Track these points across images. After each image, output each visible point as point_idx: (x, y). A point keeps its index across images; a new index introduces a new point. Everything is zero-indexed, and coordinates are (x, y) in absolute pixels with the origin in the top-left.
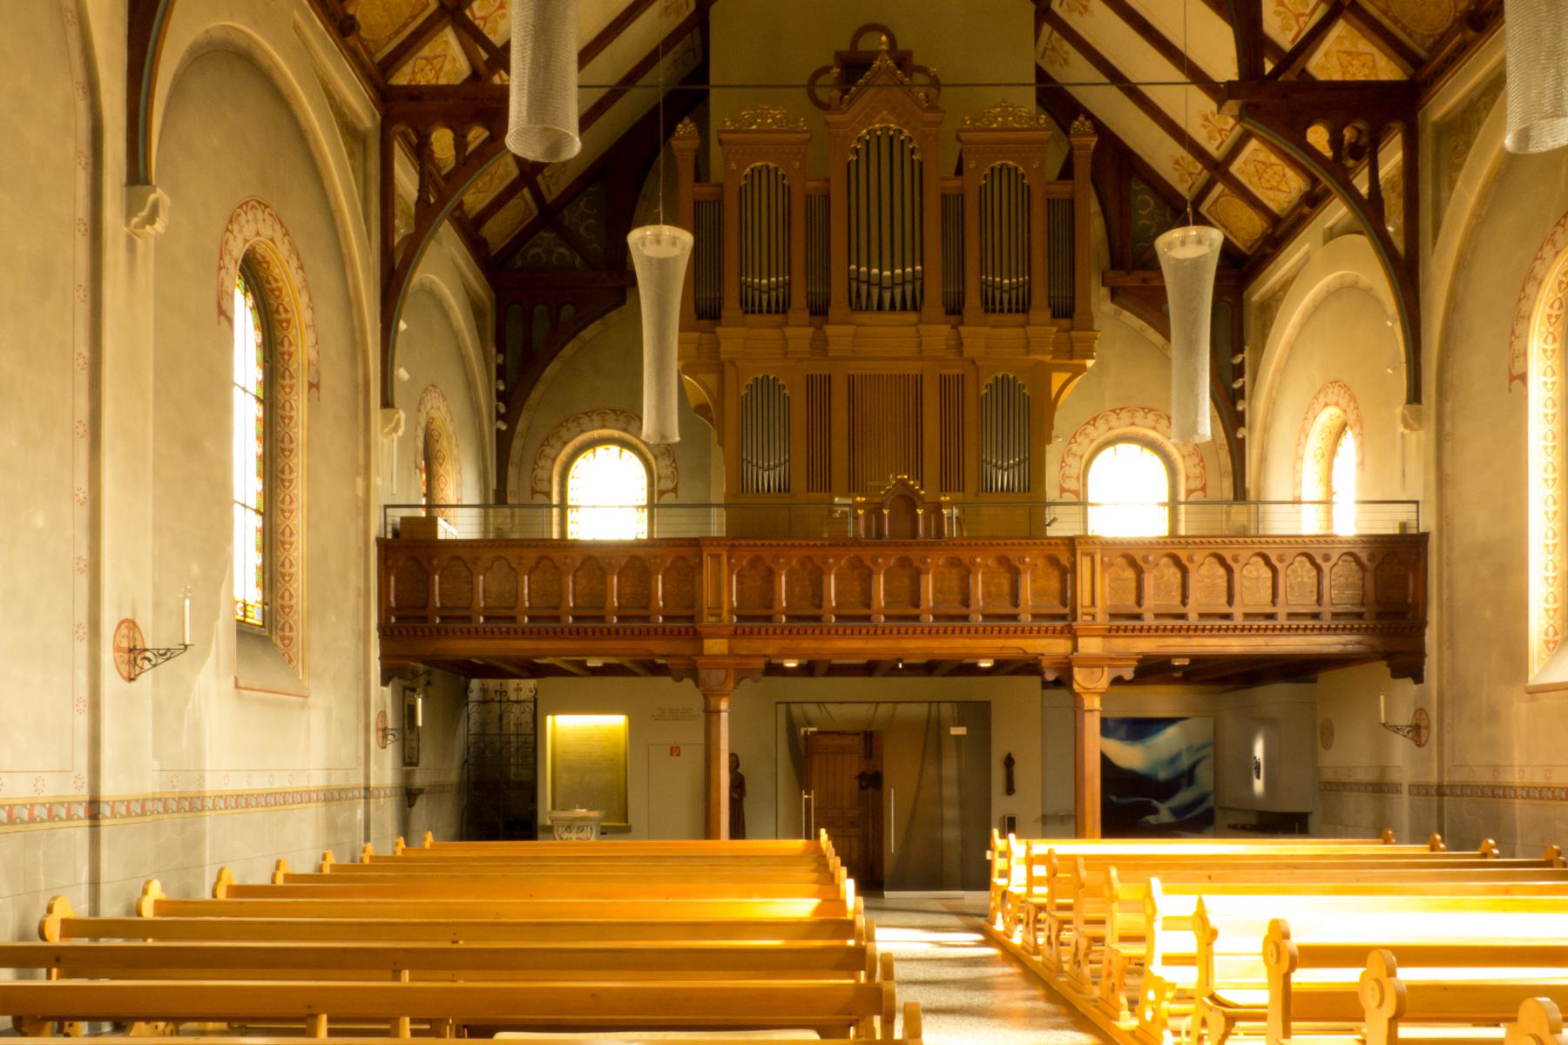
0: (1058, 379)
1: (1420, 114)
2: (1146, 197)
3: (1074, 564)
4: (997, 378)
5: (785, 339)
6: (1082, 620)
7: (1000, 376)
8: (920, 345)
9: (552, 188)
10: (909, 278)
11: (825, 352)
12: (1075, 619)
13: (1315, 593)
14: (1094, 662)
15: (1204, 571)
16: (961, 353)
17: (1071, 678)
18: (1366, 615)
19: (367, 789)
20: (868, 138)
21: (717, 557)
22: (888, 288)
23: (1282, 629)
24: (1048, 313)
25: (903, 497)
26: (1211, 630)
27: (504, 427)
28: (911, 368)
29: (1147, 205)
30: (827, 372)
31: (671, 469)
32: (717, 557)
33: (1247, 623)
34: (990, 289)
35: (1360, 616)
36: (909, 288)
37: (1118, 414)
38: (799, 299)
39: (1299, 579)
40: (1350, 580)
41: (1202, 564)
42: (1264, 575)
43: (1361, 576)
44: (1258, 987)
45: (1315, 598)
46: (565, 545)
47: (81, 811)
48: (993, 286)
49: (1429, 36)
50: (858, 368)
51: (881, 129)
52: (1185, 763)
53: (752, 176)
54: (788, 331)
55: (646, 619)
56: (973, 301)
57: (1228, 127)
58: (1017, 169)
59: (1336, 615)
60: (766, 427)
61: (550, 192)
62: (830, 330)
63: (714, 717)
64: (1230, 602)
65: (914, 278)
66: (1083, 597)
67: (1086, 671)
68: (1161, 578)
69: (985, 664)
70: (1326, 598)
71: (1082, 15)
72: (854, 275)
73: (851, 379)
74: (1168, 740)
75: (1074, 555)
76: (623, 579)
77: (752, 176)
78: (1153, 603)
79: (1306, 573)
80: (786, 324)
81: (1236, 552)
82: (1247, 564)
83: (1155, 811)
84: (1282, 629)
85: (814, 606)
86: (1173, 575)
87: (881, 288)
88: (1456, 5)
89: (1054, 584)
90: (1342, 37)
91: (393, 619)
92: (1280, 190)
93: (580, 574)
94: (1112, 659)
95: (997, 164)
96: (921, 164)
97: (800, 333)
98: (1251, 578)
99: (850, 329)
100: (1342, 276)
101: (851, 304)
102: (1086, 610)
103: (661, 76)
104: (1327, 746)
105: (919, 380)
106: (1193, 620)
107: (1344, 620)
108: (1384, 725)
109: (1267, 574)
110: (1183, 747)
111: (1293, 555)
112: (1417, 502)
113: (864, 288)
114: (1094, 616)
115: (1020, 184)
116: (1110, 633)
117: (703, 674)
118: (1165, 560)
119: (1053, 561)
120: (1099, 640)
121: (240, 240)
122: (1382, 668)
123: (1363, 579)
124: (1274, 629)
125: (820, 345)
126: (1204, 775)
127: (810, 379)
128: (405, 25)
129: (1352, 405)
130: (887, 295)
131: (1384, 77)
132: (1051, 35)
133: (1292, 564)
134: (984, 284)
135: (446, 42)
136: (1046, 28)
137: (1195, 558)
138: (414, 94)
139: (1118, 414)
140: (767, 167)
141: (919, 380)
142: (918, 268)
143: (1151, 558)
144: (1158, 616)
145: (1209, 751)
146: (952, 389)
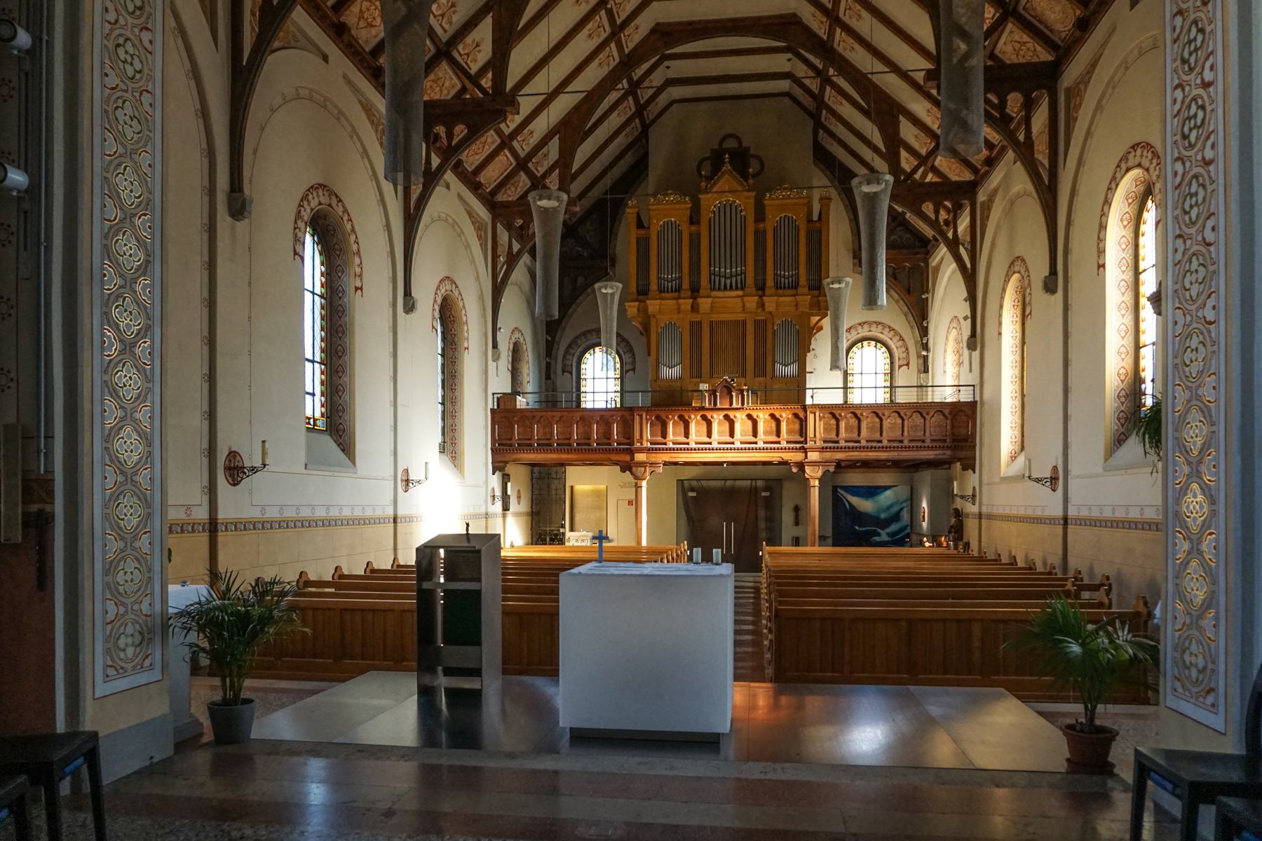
3: (806, 417)
16: (764, 310)
17: (804, 472)
19: (487, 514)
21: (641, 416)
25: (726, 387)
27: (550, 339)
28: (740, 317)
30: (699, 319)
31: (631, 360)
32: (641, 416)
33: (911, 445)
46: (327, 757)
47: (392, 520)
50: (715, 317)
52: (895, 509)
54: (681, 301)
56: (770, 283)
62: (700, 300)
65: (742, 273)
66: (810, 433)
70: (928, 433)
72: (712, 272)
73: (711, 322)
74: (887, 497)
75: (806, 412)
80: (679, 298)
83: (879, 535)
86: (854, 421)
89: (797, 426)
95: (783, 215)
96: (745, 217)
99: (710, 300)
103: (628, 160)
105: (744, 322)
106: (863, 443)
107: (939, 442)
112: (974, 386)
113: (717, 278)
116: (822, 450)
117: (634, 469)
121: (309, 210)
124: (902, 447)
125: (695, 308)
126: (905, 515)
127: (692, 323)
128: (502, 174)
130: (728, 281)
131: (968, 179)
134: (775, 274)
138: (506, 205)
141: (744, 322)
142: (743, 268)
146: (761, 326)
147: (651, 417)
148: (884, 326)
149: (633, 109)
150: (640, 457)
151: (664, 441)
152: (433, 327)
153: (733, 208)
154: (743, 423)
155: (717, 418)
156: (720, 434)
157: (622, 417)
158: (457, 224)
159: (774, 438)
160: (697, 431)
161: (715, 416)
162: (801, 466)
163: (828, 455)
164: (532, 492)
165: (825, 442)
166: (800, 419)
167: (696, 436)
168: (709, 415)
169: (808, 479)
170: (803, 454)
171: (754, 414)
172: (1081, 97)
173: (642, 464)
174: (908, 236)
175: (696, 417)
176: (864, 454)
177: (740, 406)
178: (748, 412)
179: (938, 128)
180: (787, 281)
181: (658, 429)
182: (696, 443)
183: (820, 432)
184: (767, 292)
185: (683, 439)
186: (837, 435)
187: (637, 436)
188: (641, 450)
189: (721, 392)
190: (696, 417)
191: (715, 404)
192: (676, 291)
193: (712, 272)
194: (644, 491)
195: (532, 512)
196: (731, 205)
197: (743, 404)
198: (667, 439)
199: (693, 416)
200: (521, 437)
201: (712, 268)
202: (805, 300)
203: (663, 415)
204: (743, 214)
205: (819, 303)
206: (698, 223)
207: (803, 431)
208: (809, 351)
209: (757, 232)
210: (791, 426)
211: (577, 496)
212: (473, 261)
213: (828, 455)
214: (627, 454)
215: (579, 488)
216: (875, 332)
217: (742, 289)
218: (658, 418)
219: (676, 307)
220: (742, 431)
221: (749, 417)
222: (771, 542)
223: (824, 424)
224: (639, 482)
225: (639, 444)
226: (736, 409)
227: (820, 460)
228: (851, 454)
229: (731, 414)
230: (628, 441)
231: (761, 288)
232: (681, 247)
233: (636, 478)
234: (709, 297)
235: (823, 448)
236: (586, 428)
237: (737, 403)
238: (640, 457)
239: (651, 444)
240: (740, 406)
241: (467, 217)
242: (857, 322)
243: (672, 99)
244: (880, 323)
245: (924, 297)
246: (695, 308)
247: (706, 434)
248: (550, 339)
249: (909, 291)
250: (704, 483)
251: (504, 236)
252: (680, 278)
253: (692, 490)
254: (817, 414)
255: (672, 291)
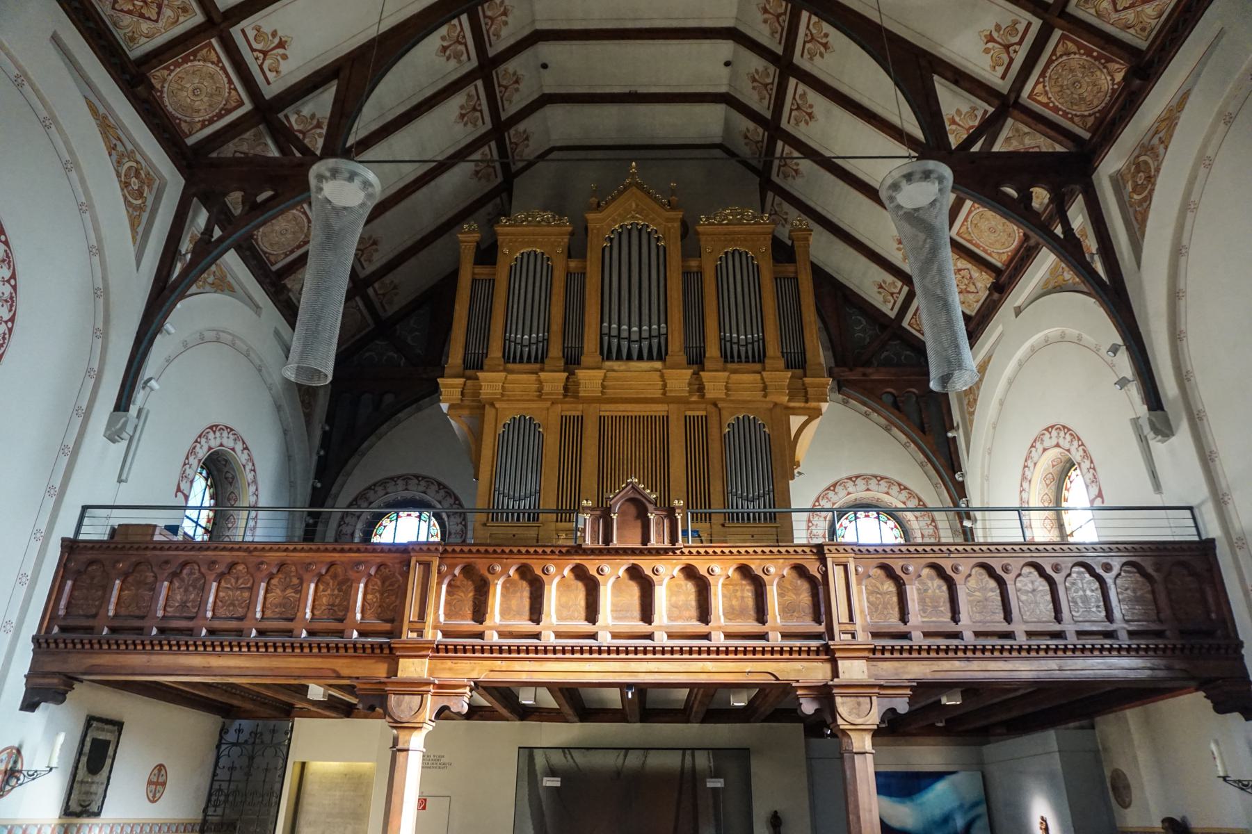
0: (796, 422)
1: (1094, 177)
2: (859, 318)
3: (825, 575)
4: (738, 418)
5: (540, 382)
6: (841, 639)
7: (741, 417)
8: (665, 386)
9: (387, 307)
10: (654, 333)
11: (576, 396)
12: (832, 638)
13: (1102, 608)
14: (858, 689)
15: (972, 582)
16: (703, 396)
17: (833, 711)
18: (1168, 633)
20: (620, 230)
22: (637, 341)
23: (1074, 650)
24: (781, 363)
26: (992, 651)
28: (659, 410)
29: (860, 322)
30: (579, 413)
31: (460, 527)
32: (427, 566)
34: (728, 344)
35: (1159, 634)
36: (655, 341)
37: (854, 482)
38: (555, 351)
39: (1081, 593)
40: (1139, 593)
41: (970, 575)
42: (1041, 588)
43: (1150, 588)
44: (446, 386)
45: (1103, 614)
48: (731, 341)
49: (1090, 115)
50: (609, 410)
51: (631, 224)
53: (522, 259)
55: (340, 633)
56: (713, 350)
57: (897, 291)
58: (747, 253)
59: (1132, 634)
60: (524, 472)
61: (385, 311)
62: (581, 374)
63: (401, 756)
64: (1008, 617)
67: (850, 701)
68: (926, 590)
69: (739, 702)
71: (807, 124)
73: (601, 419)
74: (939, 797)
76: (321, 587)
77: (522, 259)
78: (920, 619)
79: (1090, 588)
81: (1006, 561)
82: (1019, 575)
84: (1074, 650)
85: (531, 620)
86: (937, 588)
87: (630, 341)
88: (1113, 80)
89: (805, 598)
90: (1010, 137)
91: (56, 630)
92: (969, 292)
93: (274, 581)
94: (881, 687)
95: (730, 249)
96: (665, 248)
97: (554, 380)
98: (1028, 592)
100: (1046, 336)
101: (602, 353)
102: (843, 628)
104: (1125, 805)
108: (1225, 778)
109: (1043, 586)
110: (956, 804)
111: (1070, 565)
114: (854, 637)
115: (750, 265)
116: (874, 654)
118: (926, 572)
119: (800, 570)
120: (863, 663)
122: (1194, 704)
123: (1153, 592)
125: (570, 390)
127: (564, 420)
128: (292, 252)
129: (1076, 443)
132: (774, 199)
133: (1069, 575)
134: (722, 340)
135: (266, 145)
136: (770, 195)
137: (960, 568)
139: (854, 482)
140: (535, 252)
143: (911, 569)
144: (927, 635)
145: (982, 809)
146: (696, 429)
147: (452, 567)
148: (891, 482)
149: (474, 63)
150: (411, 668)
151: (478, 628)
152: (179, 490)
153: (645, 237)
154: (672, 592)
155: (611, 574)
156: (618, 611)
157: (380, 566)
158: (29, 80)
159: (752, 626)
160: (561, 607)
161: (607, 570)
162: (825, 694)
163: (888, 670)
164: (214, 774)
165: (875, 635)
166: (811, 580)
167: (560, 618)
168: (591, 566)
169: (844, 732)
170: (828, 666)
171: (701, 567)
172: (974, 395)
173: (416, 687)
174: (908, 353)
175: (560, 569)
176: (975, 665)
177: (667, 545)
178: (685, 561)
179: (905, 259)
180: (743, 349)
181: (467, 596)
182: (559, 635)
183: (862, 612)
184: (707, 364)
185: (528, 626)
186: (904, 617)
187: (411, 612)
188: (416, 650)
189: (622, 513)
190: (560, 569)
191: (608, 539)
192: (536, 361)
193: (606, 331)
194: (413, 766)
195: (205, 821)
196: (640, 231)
197: (673, 539)
198: (487, 623)
199: (552, 569)
200: (123, 612)
201: (606, 324)
202: (781, 377)
203: (481, 564)
204: (662, 243)
205: (805, 388)
206: (583, 256)
207: (820, 607)
208: (793, 478)
209: (686, 274)
210: (791, 597)
211: (311, 786)
212: (86, 207)
213: (888, 670)
214: (382, 659)
215: (321, 767)
216: (877, 493)
217: (660, 358)
218: (468, 571)
219: (535, 387)
220: (673, 606)
221: (690, 572)
222: (153, 535)
223: (870, 593)
224: (402, 735)
225: (413, 635)
226: (658, 552)
227: (872, 681)
228: (946, 665)
229: (646, 565)
230: (387, 626)
231: (697, 360)
232: (549, 296)
233: (398, 725)
234: (600, 368)
235: (874, 651)
236: (289, 592)
237: (660, 534)
238: (411, 668)
239: (445, 635)
240: (667, 545)
241: (96, 131)
242: (845, 475)
243: (552, 144)
244: (882, 478)
245: (950, 435)
246: (570, 390)
247: (583, 613)
248: (319, 485)
249: (923, 430)
250: (581, 759)
251: (201, 219)
252: (547, 341)
253: (552, 772)
254: (851, 568)
255: (529, 361)
